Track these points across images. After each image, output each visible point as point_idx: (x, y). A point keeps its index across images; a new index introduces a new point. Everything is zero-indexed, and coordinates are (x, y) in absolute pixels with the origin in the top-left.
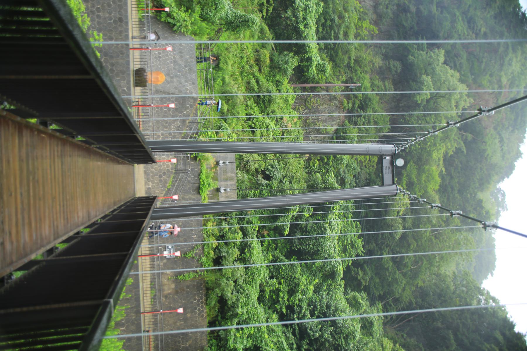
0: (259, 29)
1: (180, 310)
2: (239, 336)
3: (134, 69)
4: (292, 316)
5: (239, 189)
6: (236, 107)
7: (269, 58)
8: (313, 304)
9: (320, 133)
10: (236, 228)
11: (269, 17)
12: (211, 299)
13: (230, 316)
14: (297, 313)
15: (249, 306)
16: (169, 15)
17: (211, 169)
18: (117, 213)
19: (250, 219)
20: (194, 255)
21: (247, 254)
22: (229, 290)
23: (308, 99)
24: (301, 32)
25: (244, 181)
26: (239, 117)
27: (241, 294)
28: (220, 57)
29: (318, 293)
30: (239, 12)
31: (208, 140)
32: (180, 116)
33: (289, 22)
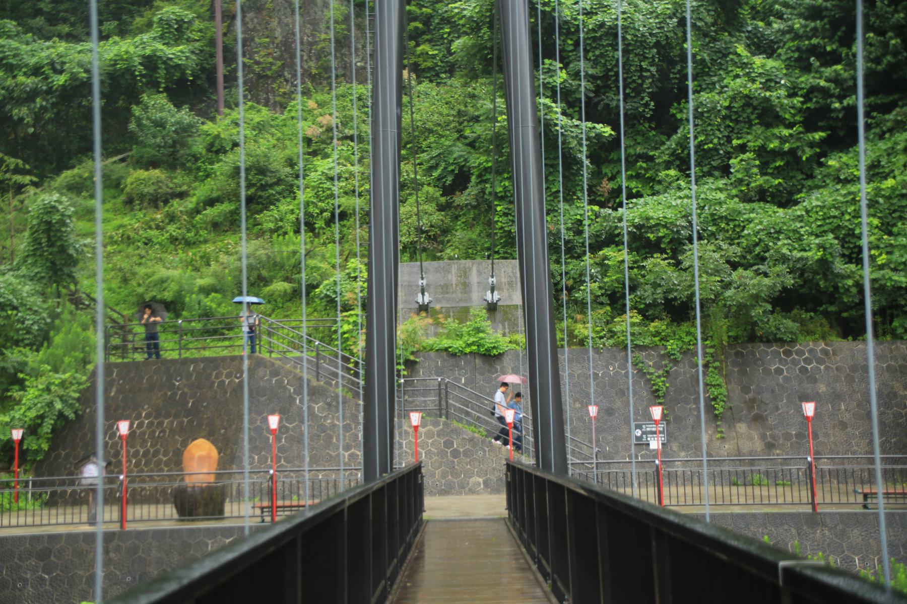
0: (70, 195)
1: (809, 409)
2: (884, 256)
3: (177, 520)
4: (833, 115)
5: (491, 253)
6: (278, 260)
7: (147, 170)
8: (804, 56)
9: (347, 38)
10: (592, 261)
11: (36, 167)
12: (779, 329)
13: (826, 281)
14: (829, 101)
15: (802, 231)
16: (32, 430)
17: (438, 324)
18: (548, 562)
19: (570, 225)
20: (661, 372)
21: (660, 234)
22: (755, 281)
23: (256, 68)
24: (74, 84)
25: (470, 240)
26: (303, 252)
27: (768, 250)
28: (148, 297)
29: (777, 42)
30: (22, 247)
31: (364, 330)
32: (301, 401)
33: (48, 116)
